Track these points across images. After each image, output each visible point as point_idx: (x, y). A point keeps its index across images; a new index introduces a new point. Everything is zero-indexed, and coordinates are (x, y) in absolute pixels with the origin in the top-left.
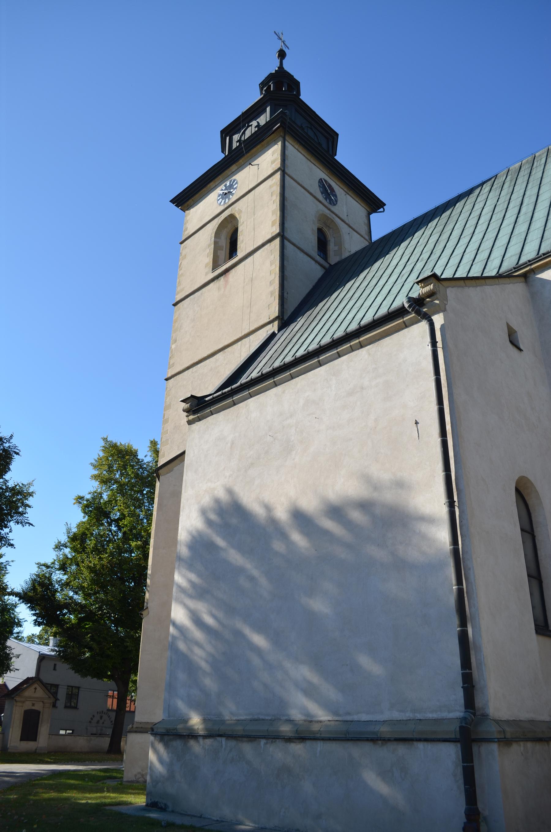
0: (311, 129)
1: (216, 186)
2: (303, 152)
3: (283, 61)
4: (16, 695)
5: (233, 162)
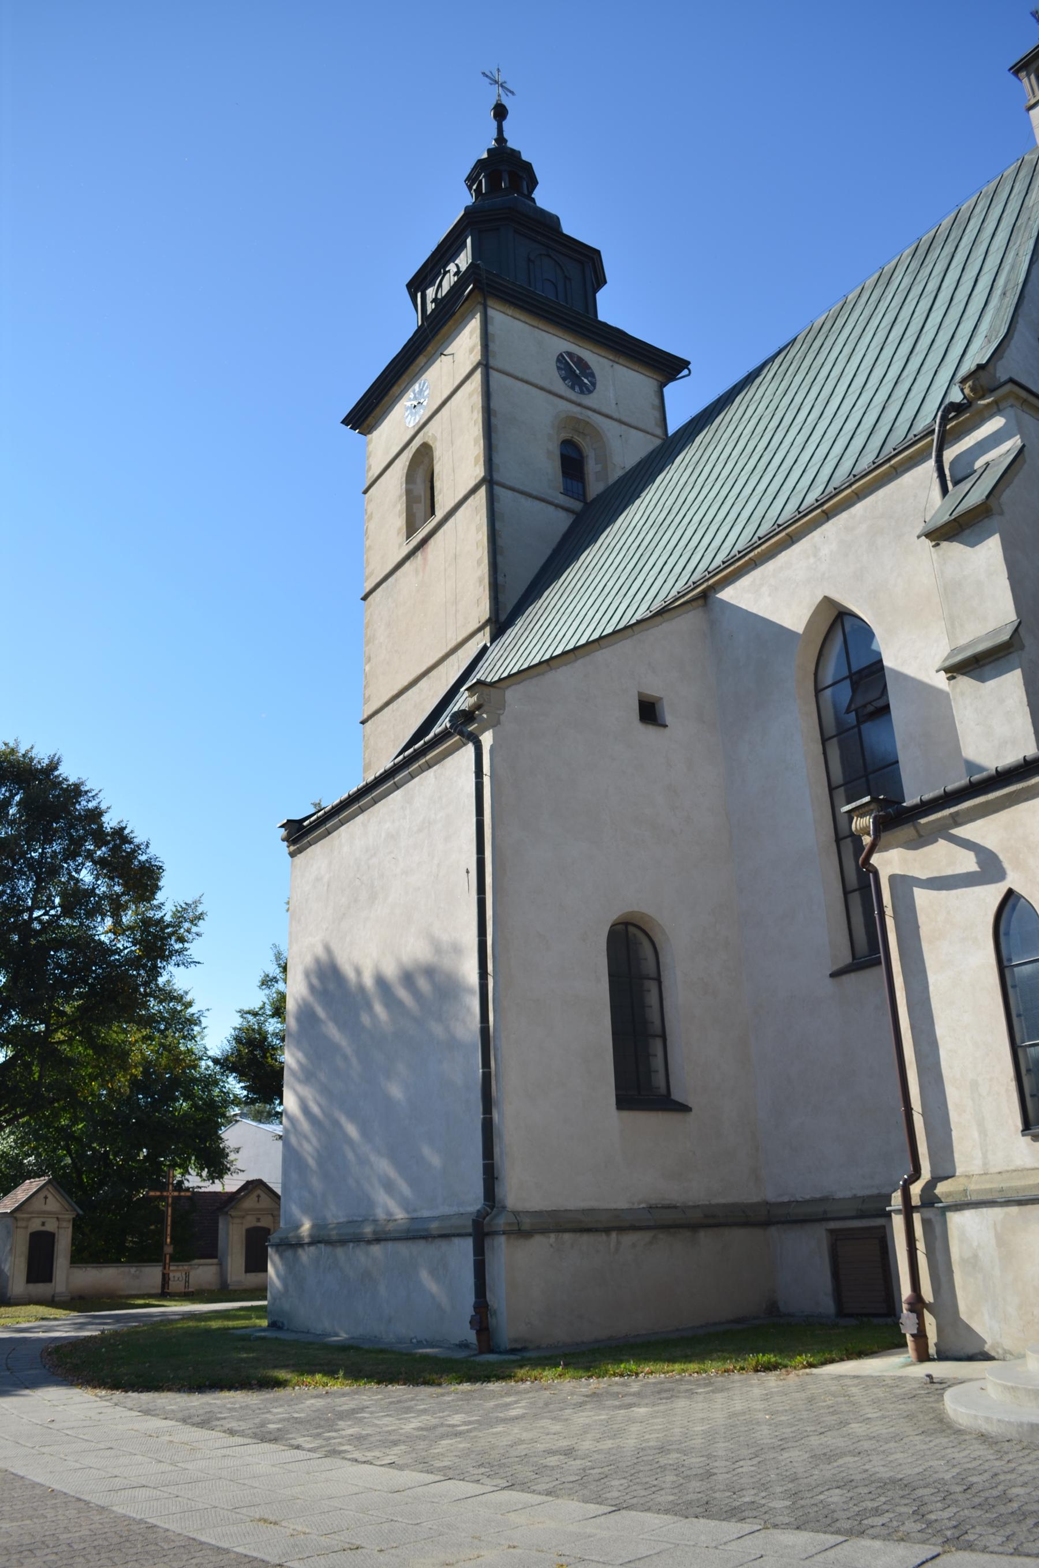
0: (549, 256)
1: (401, 392)
2: (522, 318)
3: (503, 123)
4: (232, 1208)
5: (418, 351)
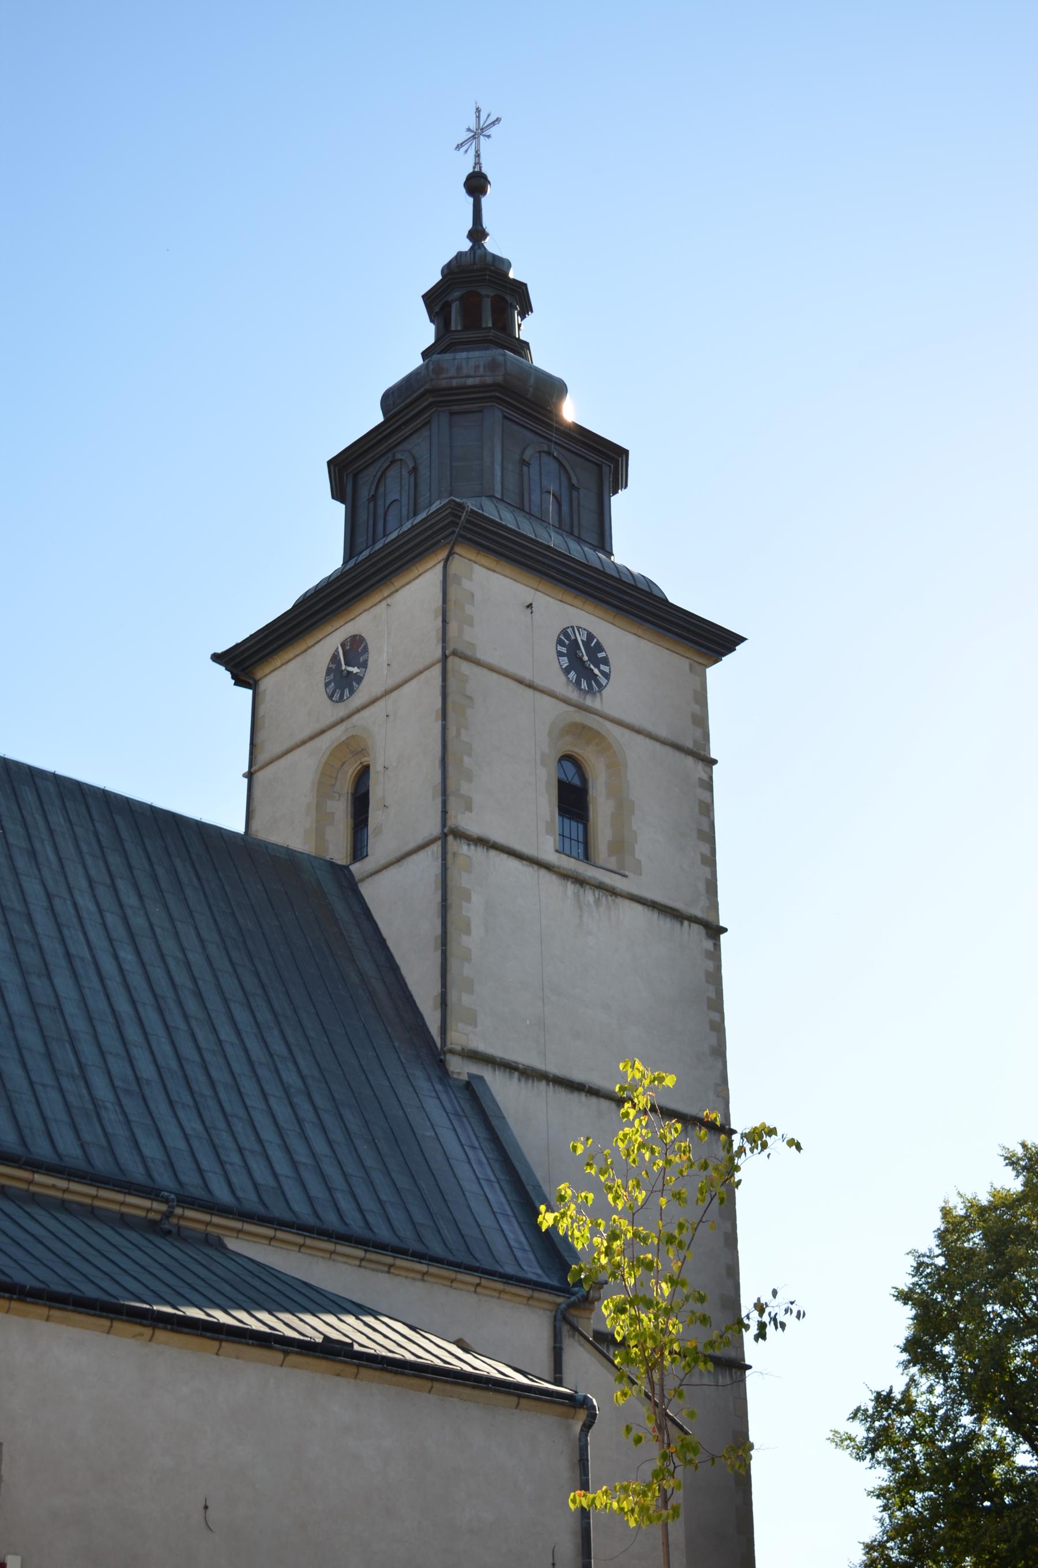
0: (549, 453)
2: (291, 655)
